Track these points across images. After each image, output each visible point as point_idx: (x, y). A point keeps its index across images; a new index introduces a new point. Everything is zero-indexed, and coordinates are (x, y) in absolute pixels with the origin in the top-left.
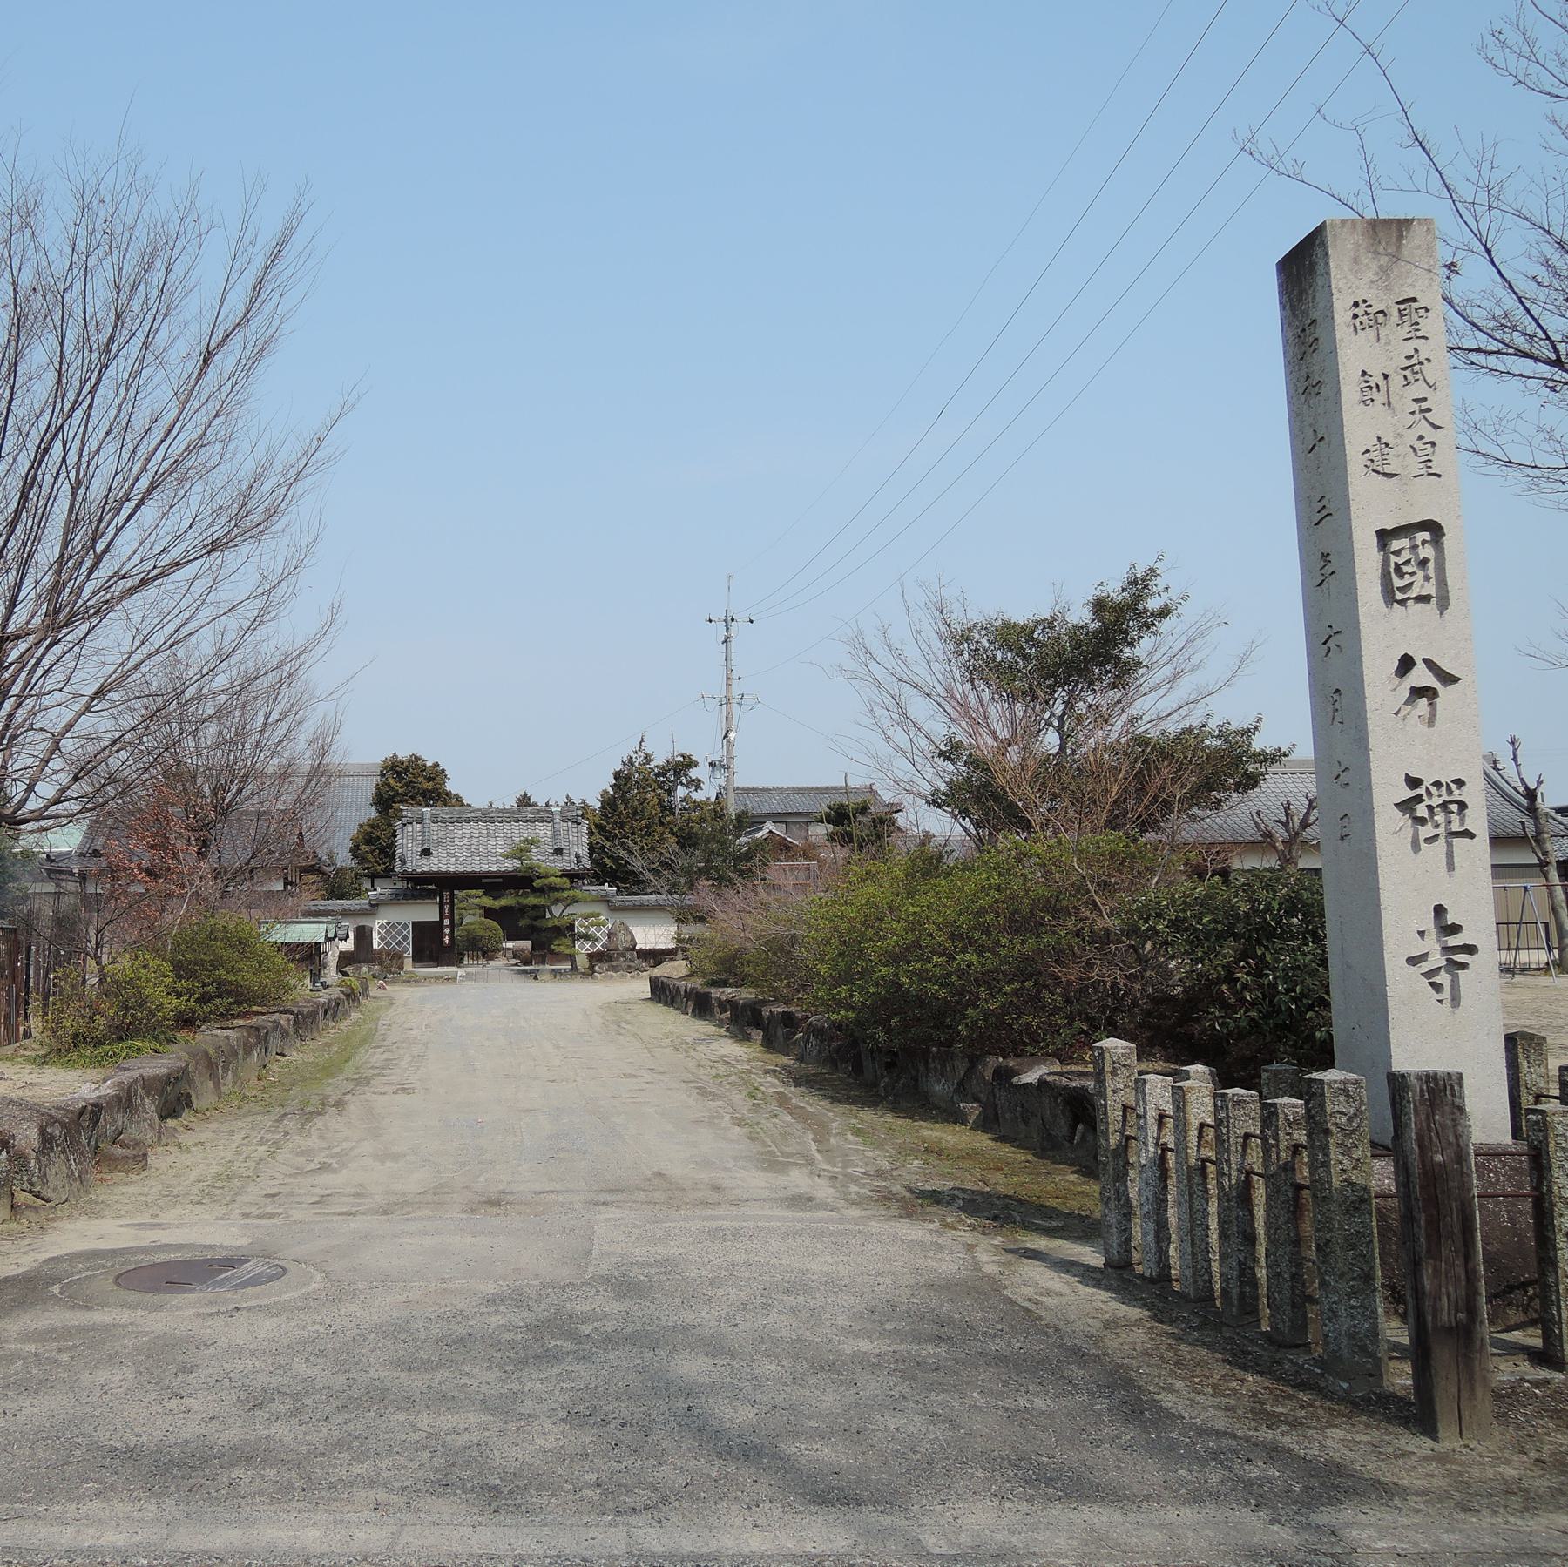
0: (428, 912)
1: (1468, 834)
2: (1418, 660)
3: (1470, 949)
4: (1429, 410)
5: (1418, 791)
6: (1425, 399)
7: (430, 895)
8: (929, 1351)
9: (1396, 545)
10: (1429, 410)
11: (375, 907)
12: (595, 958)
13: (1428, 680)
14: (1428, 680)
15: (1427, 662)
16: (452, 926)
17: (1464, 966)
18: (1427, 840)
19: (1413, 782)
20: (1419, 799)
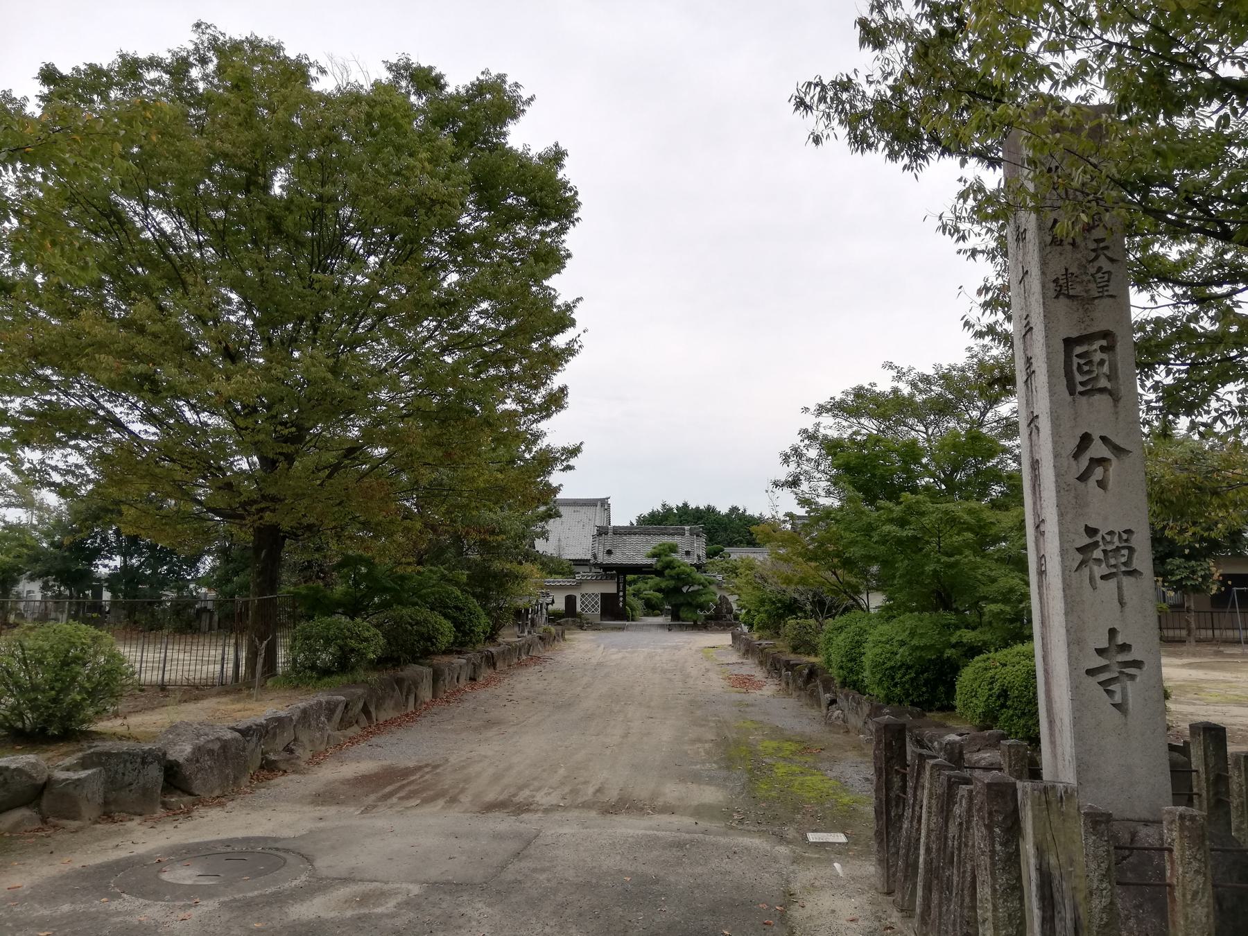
0: (611, 588)
1: (1133, 573)
2: (1096, 437)
3: (1137, 664)
4: (1106, 248)
5: (1095, 539)
6: (1103, 240)
7: (612, 577)
8: (1196, 801)
9: (1079, 350)
10: (1106, 248)
11: (579, 584)
12: (708, 618)
13: (1105, 452)
14: (1105, 452)
15: (1103, 439)
16: (624, 596)
17: (1132, 677)
18: (1103, 578)
19: (1091, 532)
20: (1096, 544)
